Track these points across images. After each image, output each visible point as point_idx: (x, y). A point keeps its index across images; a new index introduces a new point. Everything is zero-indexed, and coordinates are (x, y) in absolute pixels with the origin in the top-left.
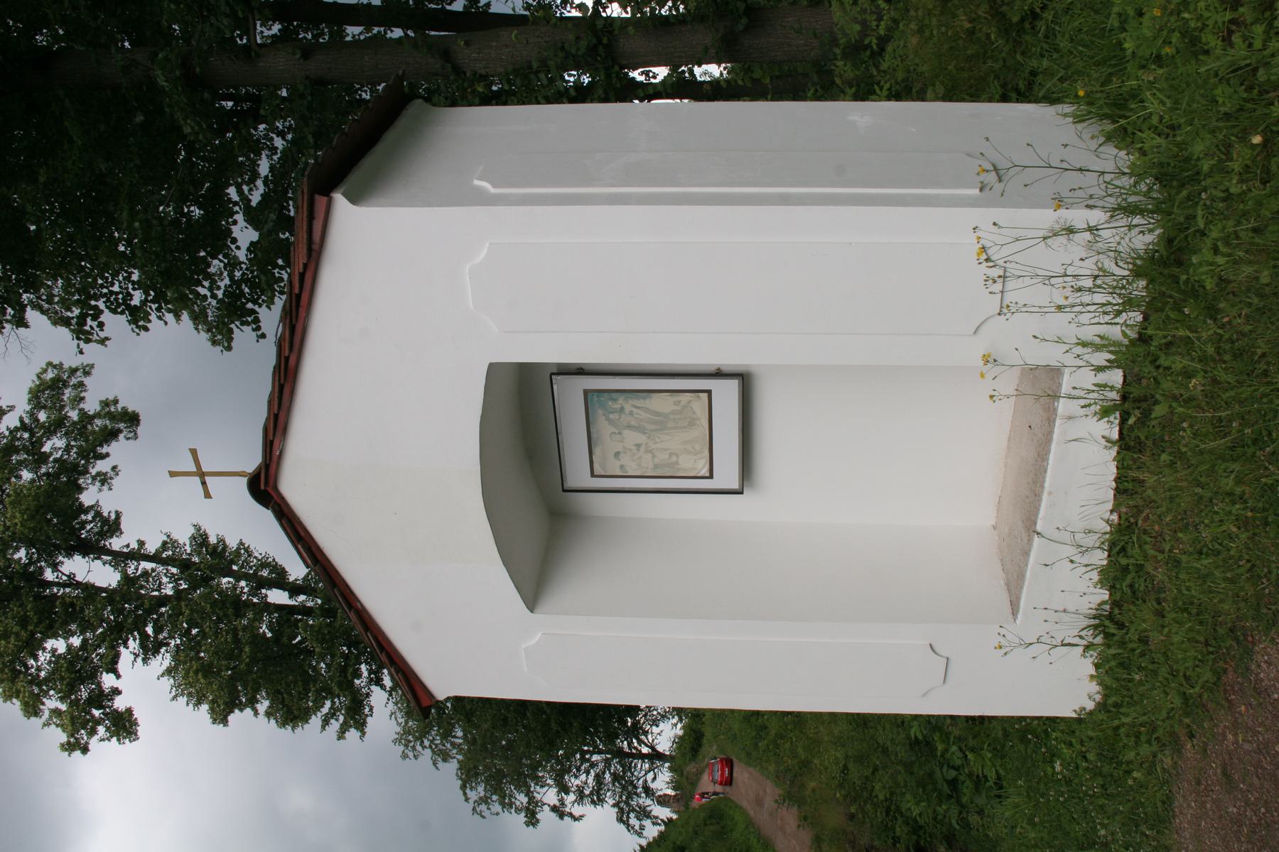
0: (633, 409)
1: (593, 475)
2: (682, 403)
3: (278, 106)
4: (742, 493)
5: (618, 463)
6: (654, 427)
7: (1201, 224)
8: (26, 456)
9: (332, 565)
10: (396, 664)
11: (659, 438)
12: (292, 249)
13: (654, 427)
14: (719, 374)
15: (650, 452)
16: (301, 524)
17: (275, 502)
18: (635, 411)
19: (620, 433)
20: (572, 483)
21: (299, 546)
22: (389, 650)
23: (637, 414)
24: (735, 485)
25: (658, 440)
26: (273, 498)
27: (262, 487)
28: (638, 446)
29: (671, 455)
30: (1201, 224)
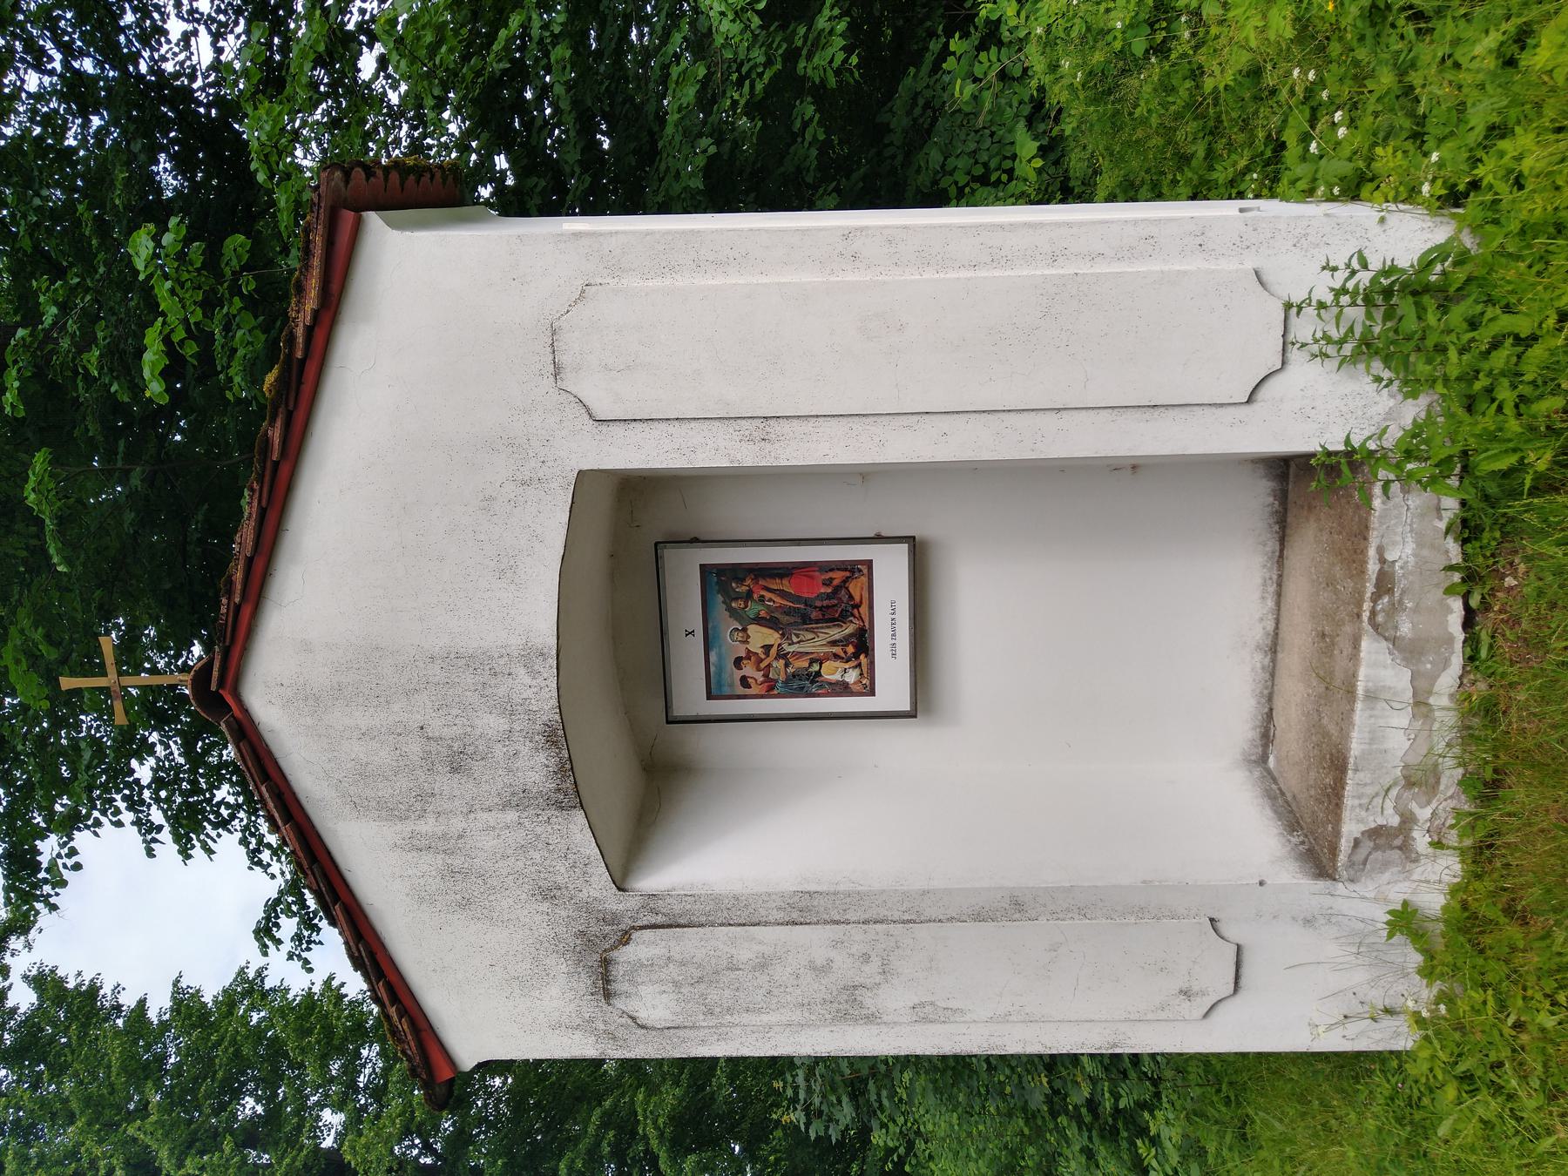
0: (763, 593)
1: (710, 696)
2: (836, 582)
3: (425, 127)
4: (915, 717)
5: (738, 674)
6: (792, 620)
7: (432, 153)
8: (315, 117)
9: (313, 826)
10: (400, 1002)
11: (797, 636)
12: (249, 505)
13: (792, 620)
14: (879, 539)
15: (784, 656)
16: (270, 753)
17: (233, 716)
18: (768, 595)
19: (744, 630)
20: (680, 709)
21: (263, 789)
22: (393, 978)
23: (770, 600)
24: (906, 706)
25: (795, 639)
26: (230, 709)
27: (213, 688)
28: (767, 648)
29: (812, 662)
30: (432, 153)
